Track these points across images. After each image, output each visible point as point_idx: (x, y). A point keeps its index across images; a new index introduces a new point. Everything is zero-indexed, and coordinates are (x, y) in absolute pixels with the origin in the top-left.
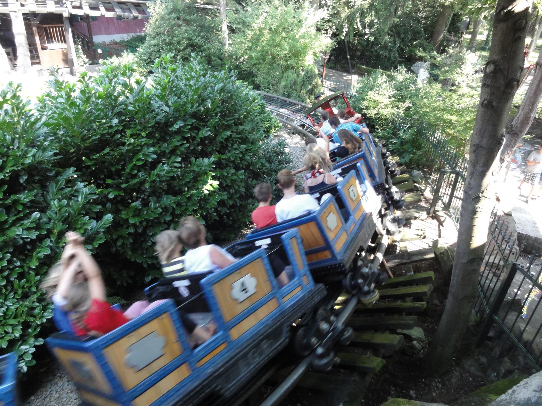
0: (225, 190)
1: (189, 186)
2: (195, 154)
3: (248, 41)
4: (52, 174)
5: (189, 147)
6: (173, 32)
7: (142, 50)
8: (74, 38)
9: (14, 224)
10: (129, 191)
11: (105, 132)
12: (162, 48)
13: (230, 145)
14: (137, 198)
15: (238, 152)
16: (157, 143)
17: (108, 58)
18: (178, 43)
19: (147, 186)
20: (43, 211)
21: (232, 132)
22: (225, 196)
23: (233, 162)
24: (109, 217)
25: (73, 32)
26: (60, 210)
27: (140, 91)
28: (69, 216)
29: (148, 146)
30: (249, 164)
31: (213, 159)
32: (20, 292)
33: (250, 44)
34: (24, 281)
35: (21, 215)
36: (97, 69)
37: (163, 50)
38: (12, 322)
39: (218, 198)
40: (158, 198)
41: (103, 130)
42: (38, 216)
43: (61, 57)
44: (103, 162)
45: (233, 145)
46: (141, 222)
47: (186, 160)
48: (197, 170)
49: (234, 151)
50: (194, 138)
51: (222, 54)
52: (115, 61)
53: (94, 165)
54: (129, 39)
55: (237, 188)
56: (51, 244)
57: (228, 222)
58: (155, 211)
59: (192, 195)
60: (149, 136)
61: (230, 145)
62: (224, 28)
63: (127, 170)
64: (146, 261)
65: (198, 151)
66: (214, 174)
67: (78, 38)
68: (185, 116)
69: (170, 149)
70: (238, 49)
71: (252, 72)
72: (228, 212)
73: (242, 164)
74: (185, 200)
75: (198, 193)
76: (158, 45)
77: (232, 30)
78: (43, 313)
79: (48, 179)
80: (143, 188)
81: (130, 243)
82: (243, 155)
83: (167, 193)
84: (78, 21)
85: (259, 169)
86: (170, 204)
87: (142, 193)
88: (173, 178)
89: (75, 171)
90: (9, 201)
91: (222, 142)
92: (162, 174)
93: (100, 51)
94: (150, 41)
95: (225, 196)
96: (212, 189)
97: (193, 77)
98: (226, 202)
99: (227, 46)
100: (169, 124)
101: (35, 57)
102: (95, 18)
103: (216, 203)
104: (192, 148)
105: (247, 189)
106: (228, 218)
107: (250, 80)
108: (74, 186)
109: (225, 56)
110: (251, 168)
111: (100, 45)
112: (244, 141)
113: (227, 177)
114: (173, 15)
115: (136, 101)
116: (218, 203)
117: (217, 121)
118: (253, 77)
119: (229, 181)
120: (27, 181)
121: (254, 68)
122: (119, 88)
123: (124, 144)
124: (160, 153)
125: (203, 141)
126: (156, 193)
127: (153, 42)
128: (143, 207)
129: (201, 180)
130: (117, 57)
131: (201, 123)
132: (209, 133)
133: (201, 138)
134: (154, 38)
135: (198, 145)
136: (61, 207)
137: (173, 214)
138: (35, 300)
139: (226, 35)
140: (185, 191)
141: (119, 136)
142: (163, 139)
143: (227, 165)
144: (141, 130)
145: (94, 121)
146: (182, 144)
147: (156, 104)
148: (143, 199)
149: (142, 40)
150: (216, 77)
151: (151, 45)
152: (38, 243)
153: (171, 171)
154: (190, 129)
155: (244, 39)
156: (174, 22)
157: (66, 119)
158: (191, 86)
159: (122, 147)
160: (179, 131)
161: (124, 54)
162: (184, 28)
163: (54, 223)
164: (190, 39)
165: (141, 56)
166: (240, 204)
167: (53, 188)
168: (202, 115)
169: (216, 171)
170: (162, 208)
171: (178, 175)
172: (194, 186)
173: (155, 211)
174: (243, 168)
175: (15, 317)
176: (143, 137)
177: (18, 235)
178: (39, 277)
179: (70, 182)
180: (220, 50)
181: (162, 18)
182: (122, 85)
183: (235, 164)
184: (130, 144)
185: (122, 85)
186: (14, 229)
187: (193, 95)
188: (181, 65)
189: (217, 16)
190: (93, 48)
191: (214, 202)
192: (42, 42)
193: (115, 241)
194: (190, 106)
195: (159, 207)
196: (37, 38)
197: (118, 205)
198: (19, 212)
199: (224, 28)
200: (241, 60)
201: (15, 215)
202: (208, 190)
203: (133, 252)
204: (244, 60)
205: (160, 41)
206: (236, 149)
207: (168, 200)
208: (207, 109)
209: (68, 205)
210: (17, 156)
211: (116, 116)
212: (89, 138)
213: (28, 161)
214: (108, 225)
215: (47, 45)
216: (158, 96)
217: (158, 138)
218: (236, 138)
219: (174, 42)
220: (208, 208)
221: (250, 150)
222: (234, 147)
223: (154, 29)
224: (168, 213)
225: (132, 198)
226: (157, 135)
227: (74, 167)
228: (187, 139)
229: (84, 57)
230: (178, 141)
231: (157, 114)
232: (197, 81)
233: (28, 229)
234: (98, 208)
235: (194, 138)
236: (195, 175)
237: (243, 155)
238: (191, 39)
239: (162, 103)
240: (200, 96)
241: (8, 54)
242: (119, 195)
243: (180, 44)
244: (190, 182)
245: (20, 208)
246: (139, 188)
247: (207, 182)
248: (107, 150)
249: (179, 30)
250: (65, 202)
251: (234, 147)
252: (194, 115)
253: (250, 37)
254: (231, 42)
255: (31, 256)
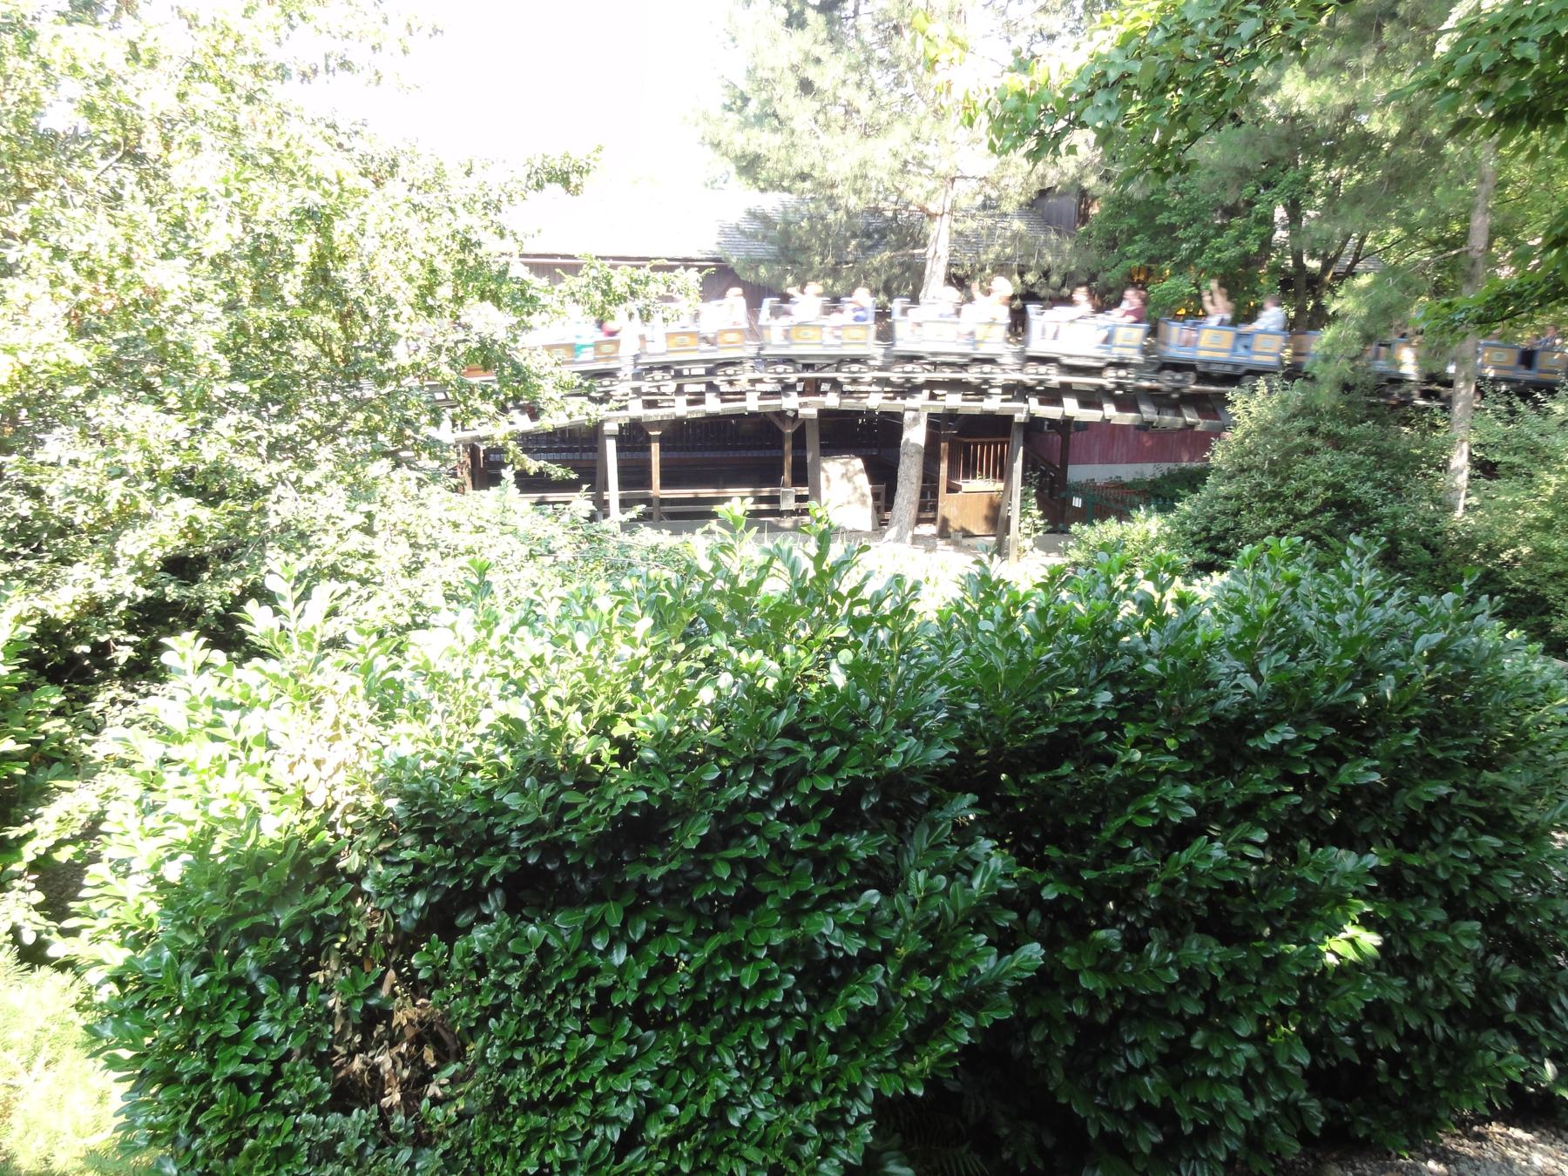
0: (1397, 973)
1: (1278, 925)
2: (1314, 831)
3: (1542, 503)
4: (922, 800)
5: (1297, 807)
6: (1290, 467)
7: (1188, 508)
8: (1025, 469)
9: (821, 904)
10: (1096, 893)
11: (1072, 720)
12: (1249, 505)
13: (1440, 828)
14: (1116, 919)
15: (1466, 855)
16: (1205, 777)
17: (1096, 522)
18: (1300, 495)
19: (1152, 891)
20: (887, 890)
21: (1455, 785)
22: (1396, 991)
23: (1445, 885)
24: (1033, 952)
25: (1025, 454)
26: (924, 899)
27: (1184, 626)
28: (939, 919)
29: (1177, 778)
30: (1504, 908)
31: (1372, 860)
32: (787, 1081)
33: (1549, 514)
34: (802, 1055)
35: (842, 887)
36: (1061, 545)
37: (1250, 512)
38: (752, 1153)
39: (1369, 990)
40: (1172, 937)
41: (1069, 715)
42: (876, 900)
43: (984, 510)
44: (1047, 798)
45: (1450, 828)
46: (1110, 994)
47: (1281, 841)
48: (1313, 879)
49: (1451, 851)
50: (1319, 783)
51: (1440, 534)
52: (1111, 529)
53: (1022, 799)
54: (1159, 475)
55: (1443, 976)
56: (883, 983)
57: (1389, 1085)
58: (1159, 972)
59: (1282, 957)
60: (1185, 752)
61: (1440, 828)
62: (1460, 460)
63: (1107, 835)
64: (1098, 1118)
65: (1324, 823)
66: (1367, 909)
67: (1034, 469)
68: (1301, 711)
69: (1240, 799)
70: (1501, 523)
71: (1543, 599)
72: (1397, 1049)
73: (1479, 899)
74: (1258, 967)
75: (1303, 956)
76: (1239, 497)
77: (1485, 469)
78: (819, 1162)
79: (910, 810)
80: (1139, 896)
81: (1067, 1047)
82: (1487, 869)
83: (1203, 927)
84: (1041, 431)
85: (1542, 931)
86: (1207, 966)
87: (1131, 909)
88: (1231, 888)
89: (973, 806)
90: (827, 847)
91: (1412, 814)
92: (1202, 866)
93: (1077, 502)
94: (1217, 486)
95: (1396, 991)
96: (1352, 955)
97: (1347, 602)
98: (1396, 1012)
99: (1459, 513)
100: (1251, 727)
101: (927, 504)
102: (1085, 426)
103: (1359, 1006)
104: (1307, 811)
105: (1479, 990)
106: (1393, 1073)
107: (1531, 620)
108: (970, 844)
109: (1446, 541)
110: (1511, 921)
111: (1079, 490)
112: (1498, 822)
113: (1412, 929)
114: (1300, 423)
115: (1168, 650)
116: (1369, 1010)
117: (1407, 743)
118: (1547, 612)
119: (1417, 945)
120: (873, 809)
121: (1551, 586)
122: (1128, 609)
123: (1110, 760)
124: (1206, 806)
125: (1346, 798)
126: (1173, 920)
127: (1223, 490)
128: (1124, 949)
129: (1320, 918)
130: (1120, 520)
131: (1353, 743)
132: (1376, 777)
133: (1343, 787)
134: (1229, 478)
135: (1330, 804)
136: (930, 892)
137: (1209, 998)
138: (813, 1118)
139: (1462, 480)
140: (1260, 937)
141: (1104, 735)
142: (1222, 767)
143: (1419, 891)
144: (1167, 732)
145: (1051, 687)
146: (1279, 795)
147: (1222, 666)
148: (1130, 926)
149: (1194, 480)
150: (1423, 611)
151: (1217, 498)
152: (856, 970)
153: (1230, 866)
154: (1311, 754)
155: (1529, 496)
156: (1298, 440)
157: (989, 672)
158: (1335, 628)
159: (1103, 767)
160: (1277, 754)
161: (1141, 514)
162: (1325, 458)
163: (904, 930)
164: (1336, 487)
165: (1183, 523)
166: (1447, 1037)
167: (921, 840)
168: (1356, 718)
169: (1378, 899)
170: (1180, 971)
171: (1246, 880)
172: (1294, 930)
173: (1159, 972)
174: (1476, 916)
175: (760, 1145)
176: (1168, 752)
177: (822, 935)
178: (836, 1057)
179: (963, 835)
180: (1435, 521)
181: (1264, 430)
182: (1141, 604)
183: (1450, 893)
184: (1128, 764)
185: (1141, 604)
186: (818, 916)
187: (1339, 659)
188: (1310, 565)
189: (1435, 427)
190: (1063, 495)
191: (1355, 1000)
192: (952, 474)
193: (1030, 1024)
194: (1324, 685)
195: (1171, 963)
196: (944, 467)
197: (1059, 924)
198: (840, 878)
199: (1460, 460)
200: (1505, 556)
201: (829, 884)
202: (1338, 956)
203: (1067, 1076)
204: (1515, 559)
205: (1247, 487)
206: (1460, 845)
207: (1204, 952)
208: (1377, 703)
209: (945, 892)
210: (871, 746)
211: (1106, 684)
212: (1030, 728)
213: (893, 763)
214: (1028, 975)
215: (960, 482)
216: (1231, 646)
217: (1207, 761)
218: (1462, 806)
219: (1287, 492)
220: (1327, 1014)
221: (1514, 857)
222: (1456, 836)
223: (1235, 455)
224: (1196, 989)
225: (1100, 914)
226: (1206, 752)
227: (975, 793)
228: (1298, 782)
229: (1036, 513)
230: (1267, 782)
231: (1220, 696)
232: (1359, 616)
233: (847, 927)
234: (1007, 918)
235: (1319, 783)
236: (1303, 896)
237: (1487, 869)
238: (1342, 487)
239: (1236, 664)
240: (1360, 660)
241: (876, 496)
242: (1071, 898)
243: (1304, 500)
244: (1280, 913)
245: (844, 870)
246: (1127, 892)
247: (1339, 929)
248: (1067, 769)
249: (1308, 462)
250: (941, 881)
251: (1456, 836)
252: (1331, 715)
253: (1551, 492)
254: (1474, 500)
255: (833, 999)
